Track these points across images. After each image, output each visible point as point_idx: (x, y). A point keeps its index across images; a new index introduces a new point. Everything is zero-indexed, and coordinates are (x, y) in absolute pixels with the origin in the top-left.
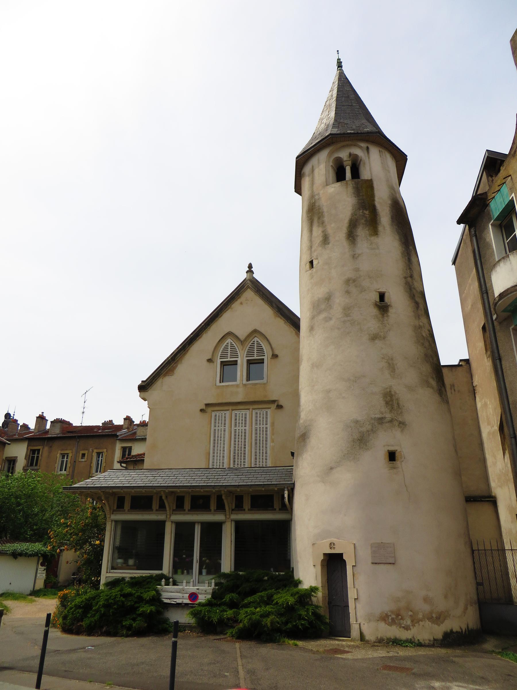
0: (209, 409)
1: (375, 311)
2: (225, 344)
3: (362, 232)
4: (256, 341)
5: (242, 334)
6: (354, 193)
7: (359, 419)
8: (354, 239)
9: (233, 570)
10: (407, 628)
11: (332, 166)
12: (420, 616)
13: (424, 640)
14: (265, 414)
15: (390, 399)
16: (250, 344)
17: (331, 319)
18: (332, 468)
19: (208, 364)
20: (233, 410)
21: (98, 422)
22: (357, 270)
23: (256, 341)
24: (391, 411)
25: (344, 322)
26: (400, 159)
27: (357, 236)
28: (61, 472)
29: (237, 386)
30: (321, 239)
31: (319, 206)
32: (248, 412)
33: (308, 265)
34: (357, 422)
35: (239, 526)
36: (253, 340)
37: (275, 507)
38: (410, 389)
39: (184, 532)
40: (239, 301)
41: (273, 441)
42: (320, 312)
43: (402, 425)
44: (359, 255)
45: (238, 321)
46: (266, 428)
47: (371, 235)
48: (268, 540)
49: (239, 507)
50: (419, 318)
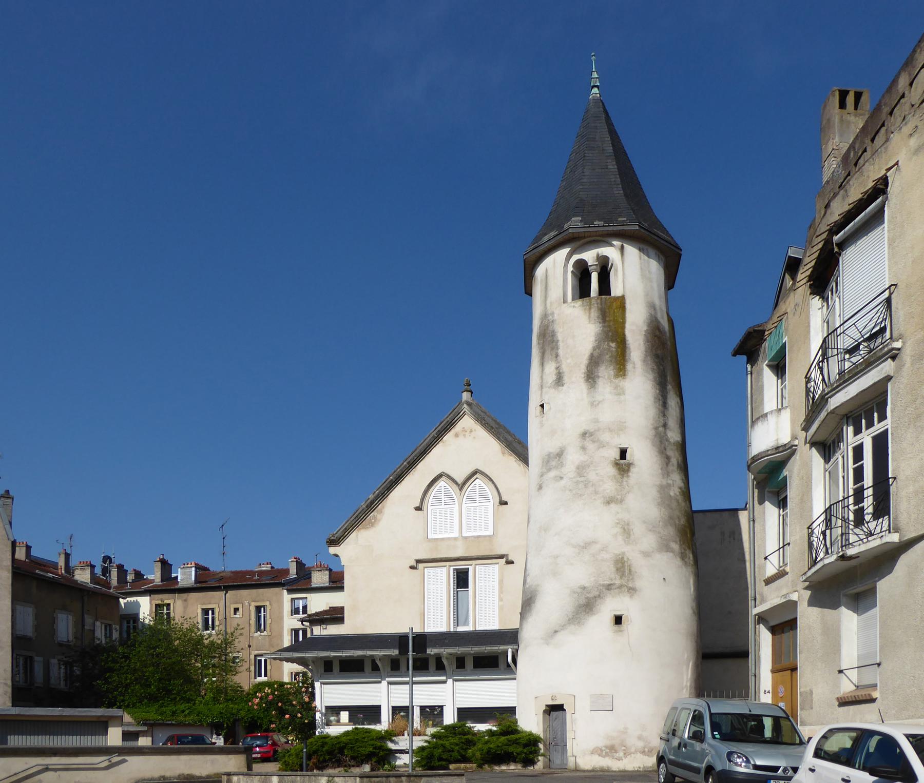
0: (420, 566)
1: (612, 471)
3: (606, 372)
6: (598, 317)
7: (587, 585)
8: (595, 382)
9: (456, 720)
10: (619, 759)
12: (633, 750)
15: (622, 566)
17: (561, 478)
18: (556, 632)
22: (596, 421)
24: (621, 578)
25: (577, 483)
27: (598, 377)
29: (455, 539)
30: (554, 377)
31: (553, 331)
34: (584, 588)
38: (646, 554)
40: (453, 432)
41: (501, 599)
42: (549, 470)
44: (600, 402)
47: (617, 376)
50: (668, 475)
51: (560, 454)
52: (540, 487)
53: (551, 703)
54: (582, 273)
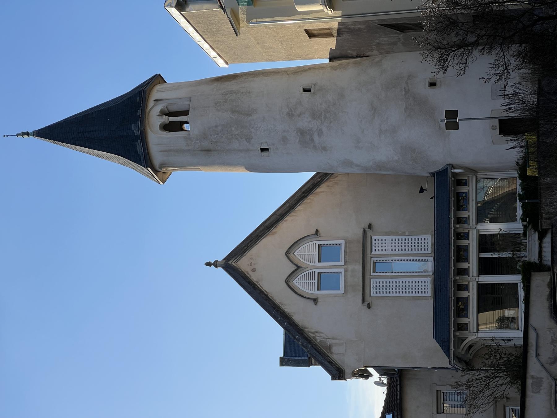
2: (300, 287)
4: (298, 254)
14: (376, 242)
19: (319, 304)
20: (371, 275)
21: (380, 414)
23: (298, 254)
26: (157, 79)
29: (346, 271)
33: (265, 154)
34: (406, 108)
36: (297, 256)
37: (467, 191)
41: (403, 234)
42: (312, 140)
43: (410, 76)
51: (302, 133)
52: (325, 149)
53: (498, 131)
54: (168, 127)
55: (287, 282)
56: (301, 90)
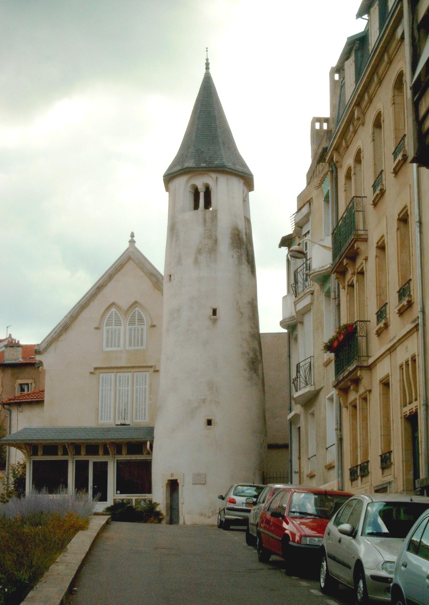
0: (97, 372)
2: (109, 314)
5: (124, 303)
11: (190, 191)
13: (78, 518)
16: (131, 315)
20: (117, 372)
26: (247, 180)
28: (48, 498)
29: (121, 352)
32: (130, 375)
35: (120, 466)
39: (81, 467)
41: (150, 399)
45: (121, 293)
46: (145, 388)
48: (136, 476)
49: (119, 452)
55: (113, 304)
56: (214, 307)
